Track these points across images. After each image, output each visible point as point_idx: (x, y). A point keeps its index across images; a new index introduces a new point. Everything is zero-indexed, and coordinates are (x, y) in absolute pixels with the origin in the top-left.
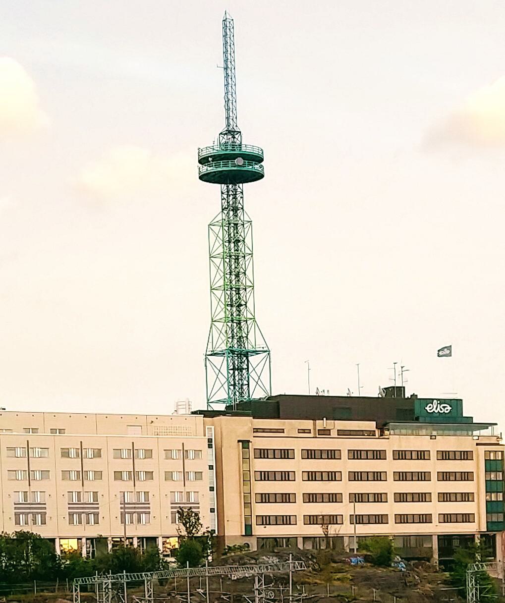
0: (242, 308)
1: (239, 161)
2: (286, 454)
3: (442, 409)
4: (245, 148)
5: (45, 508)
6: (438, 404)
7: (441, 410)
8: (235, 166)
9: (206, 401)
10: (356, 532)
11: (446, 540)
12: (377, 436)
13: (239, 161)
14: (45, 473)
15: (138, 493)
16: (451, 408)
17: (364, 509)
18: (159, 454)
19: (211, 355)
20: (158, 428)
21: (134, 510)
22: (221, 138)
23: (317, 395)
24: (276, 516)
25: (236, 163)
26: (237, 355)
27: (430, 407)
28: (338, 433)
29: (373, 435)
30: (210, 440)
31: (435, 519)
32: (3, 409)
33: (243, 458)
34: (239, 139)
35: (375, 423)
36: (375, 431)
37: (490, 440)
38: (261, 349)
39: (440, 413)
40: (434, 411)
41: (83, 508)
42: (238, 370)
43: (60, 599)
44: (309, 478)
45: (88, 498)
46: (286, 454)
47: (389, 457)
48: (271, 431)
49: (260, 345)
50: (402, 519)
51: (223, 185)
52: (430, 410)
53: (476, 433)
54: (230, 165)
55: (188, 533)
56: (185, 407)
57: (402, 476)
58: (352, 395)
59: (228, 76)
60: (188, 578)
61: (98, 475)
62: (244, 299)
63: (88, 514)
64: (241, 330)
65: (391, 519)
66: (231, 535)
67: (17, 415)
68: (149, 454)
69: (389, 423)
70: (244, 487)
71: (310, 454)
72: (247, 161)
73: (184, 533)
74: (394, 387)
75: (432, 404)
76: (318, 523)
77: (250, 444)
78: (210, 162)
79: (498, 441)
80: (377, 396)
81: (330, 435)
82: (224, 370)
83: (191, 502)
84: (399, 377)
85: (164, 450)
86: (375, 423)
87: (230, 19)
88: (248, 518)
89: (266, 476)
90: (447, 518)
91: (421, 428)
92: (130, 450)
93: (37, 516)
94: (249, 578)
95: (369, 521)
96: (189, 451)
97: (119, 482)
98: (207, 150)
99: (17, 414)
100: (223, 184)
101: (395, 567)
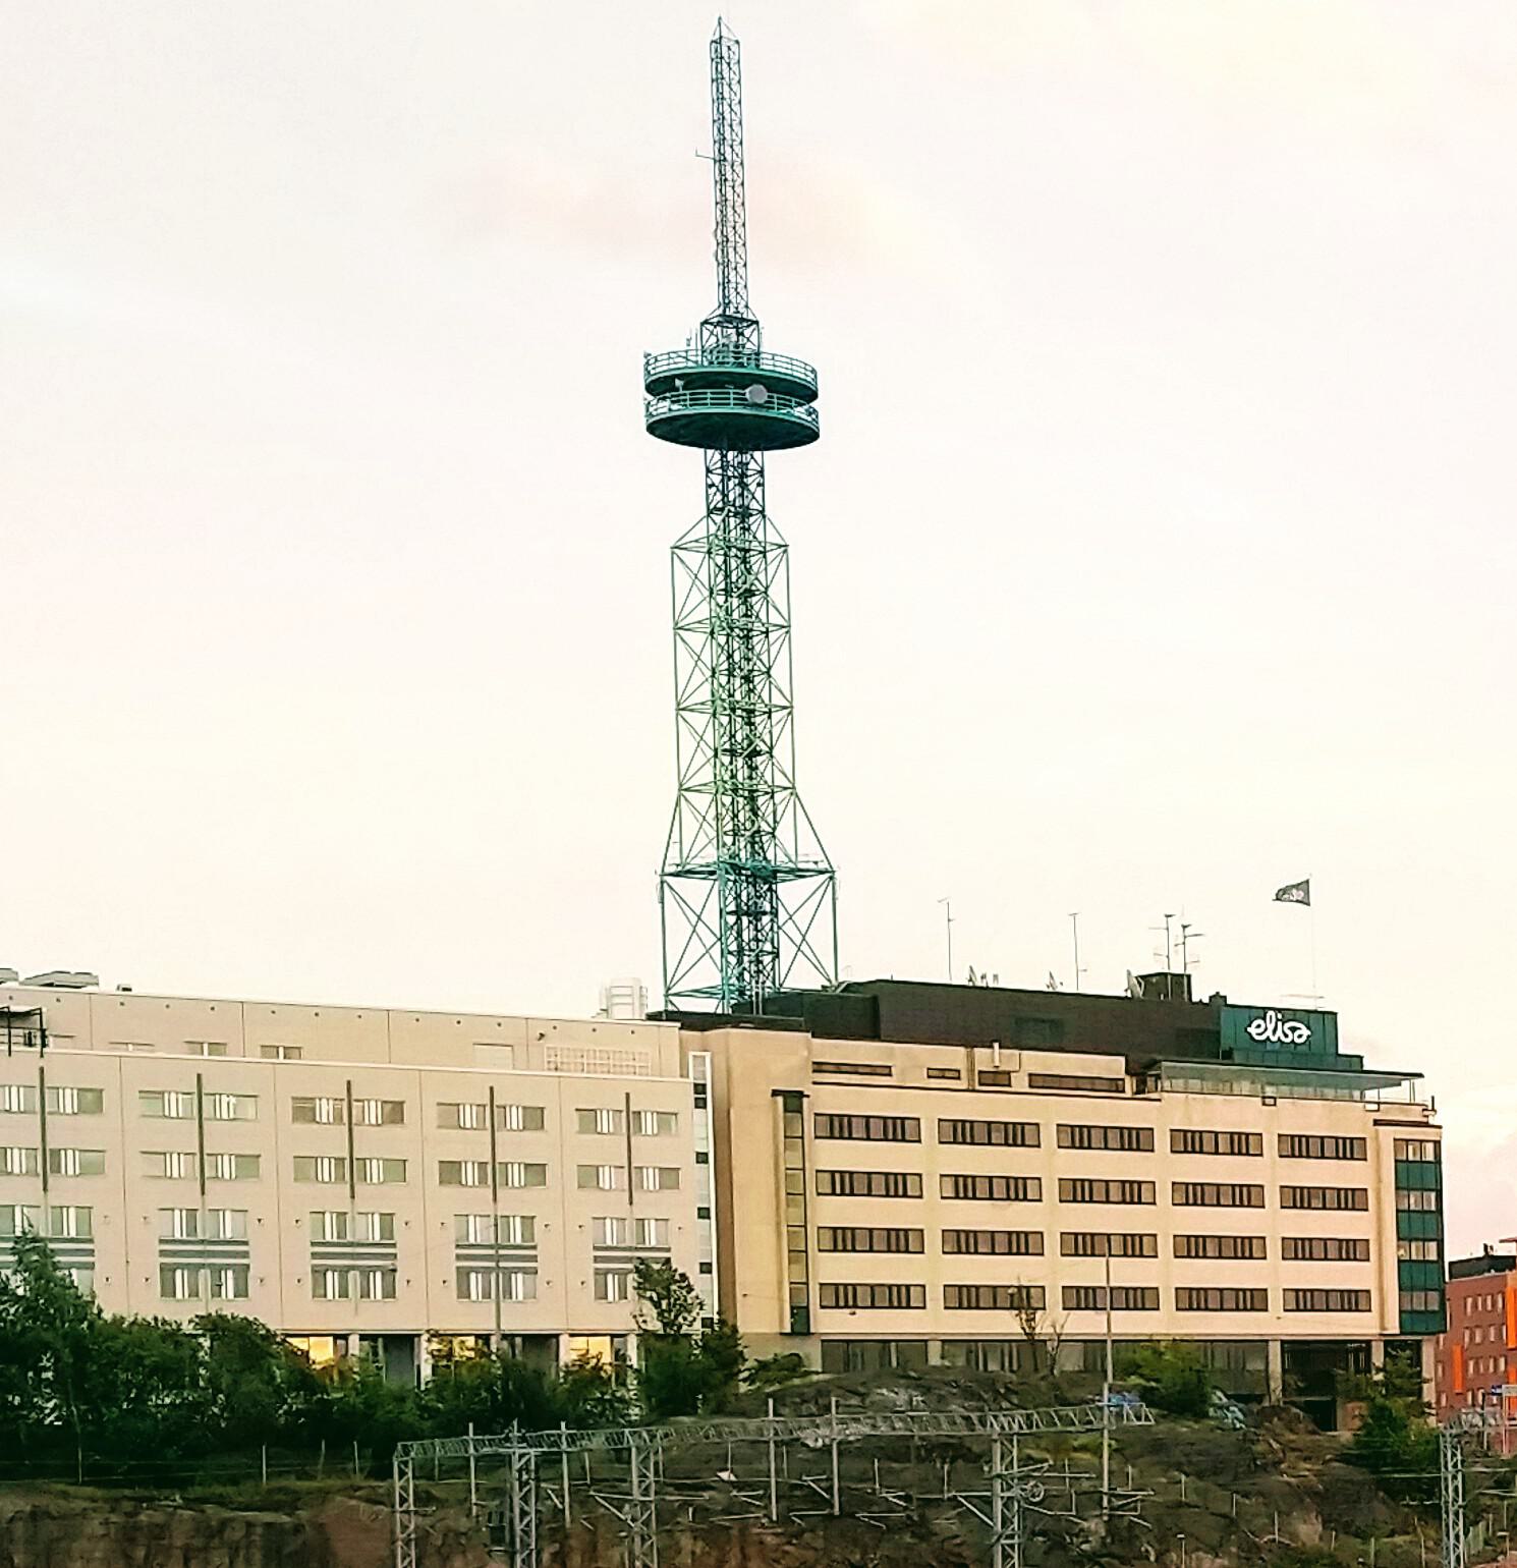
0: (759, 759)
1: (757, 393)
2: (897, 1130)
3: (1289, 1032)
4: (771, 362)
6: (1278, 1020)
7: (1286, 1036)
8: (745, 406)
9: (662, 991)
10: (1113, 1331)
11: (1299, 1352)
13: (757, 393)
14: (248, 1163)
17: (1089, 1272)
18: (561, 1120)
19: (677, 875)
20: (559, 1053)
22: (706, 334)
23: (971, 984)
25: (748, 396)
26: (747, 876)
27: (1259, 1026)
28: (1030, 1081)
29: (1117, 1091)
30: (700, 1089)
31: (1275, 1300)
32: (125, 989)
33: (786, 1137)
34: (754, 339)
35: (1122, 1059)
36: (1123, 1080)
38: (812, 866)
39: (1283, 1043)
40: (1268, 1038)
41: (352, 1256)
42: (747, 914)
43: (339, 1498)
44: (887, 1190)
46: (897, 1130)
47: (1271, 1141)
48: (854, 1069)
49: (809, 854)
50: (1194, 1299)
51: (710, 452)
53: (1371, 1095)
54: (708, 401)
55: (665, 1325)
57: (1193, 1194)
58: (1060, 989)
59: (726, 180)
60: (772, 1445)
61: (397, 1169)
62: (767, 738)
64: (756, 815)
65: (1167, 1300)
66: (755, 1331)
68: (535, 1118)
69: (1160, 1061)
70: (791, 1210)
71: (961, 1132)
72: (775, 395)
73: (656, 1326)
74: (1165, 975)
75: (1264, 1019)
76: (982, 1305)
77: (805, 1100)
78: (677, 390)
80: (1123, 994)
81: (1009, 1085)
82: (712, 917)
83: (647, 1245)
84: (1176, 952)
85: (577, 1110)
86: (1122, 1059)
87: (729, 40)
88: (799, 1288)
89: (844, 1184)
90: (1304, 1300)
91: (1240, 1077)
92: (484, 1106)
93: (223, 1273)
94: (858, 1445)
95: (1222, 1304)
96: (643, 1114)
97: (451, 1190)
98: (671, 361)
99: (168, 1002)
100: (711, 448)
101: (1217, 1418)
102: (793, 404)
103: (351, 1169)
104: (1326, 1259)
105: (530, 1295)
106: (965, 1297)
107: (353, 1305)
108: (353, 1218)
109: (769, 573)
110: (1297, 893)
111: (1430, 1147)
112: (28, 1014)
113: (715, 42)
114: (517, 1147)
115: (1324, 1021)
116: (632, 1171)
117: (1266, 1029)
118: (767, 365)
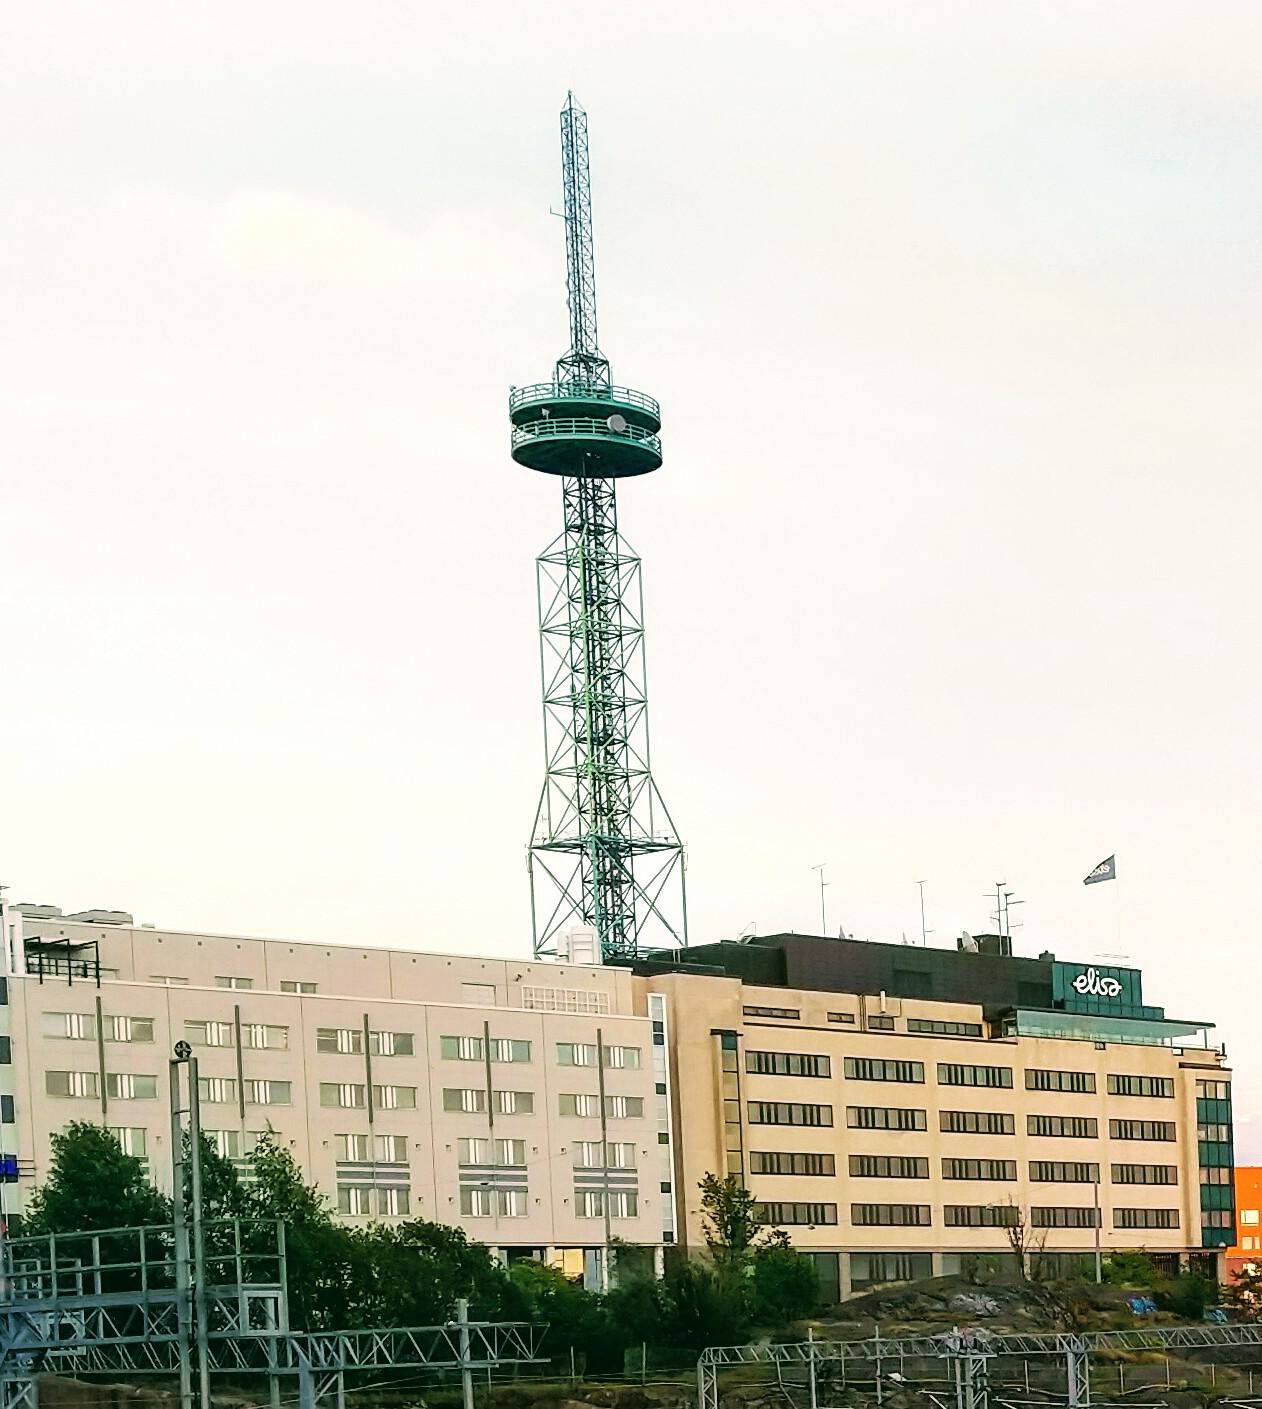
1: (615, 423)
2: (810, 1066)
3: (1105, 987)
5: (636, 1179)
6: (1096, 976)
7: (1103, 990)
8: (605, 433)
12: (986, 1038)
13: (615, 423)
15: (612, 1146)
16: (1120, 987)
17: (1074, 1195)
18: (545, 1054)
21: (371, 1181)
24: (794, 1205)
27: (1082, 981)
34: (605, 376)
36: (980, 1026)
37: (1204, 1057)
38: (664, 842)
40: (1089, 992)
45: (388, 1152)
46: (810, 1066)
49: (662, 832)
51: (567, 479)
52: (1083, 988)
56: (588, 946)
63: (384, 1189)
67: (200, 944)
68: (523, 1051)
71: (862, 1069)
75: (1086, 975)
79: (1219, 1060)
81: (893, 1029)
86: (980, 1007)
89: (769, 1114)
92: (480, 1039)
97: (454, 1116)
98: (538, 392)
100: (568, 475)
102: (645, 435)
103: (369, 1095)
104: (1145, 1183)
105: (524, 1211)
106: (959, 1216)
107: (493, 1220)
108: (372, 1140)
109: (624, 584)
110: (1105, 871)
111: (1221, 1087)
112: (83, 946)
113: (565, 112)
114: (509, 1077)
115: (1131, 979)
116: (604, 1100)
117: (1088, 984)
118: (619, 398)
